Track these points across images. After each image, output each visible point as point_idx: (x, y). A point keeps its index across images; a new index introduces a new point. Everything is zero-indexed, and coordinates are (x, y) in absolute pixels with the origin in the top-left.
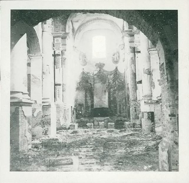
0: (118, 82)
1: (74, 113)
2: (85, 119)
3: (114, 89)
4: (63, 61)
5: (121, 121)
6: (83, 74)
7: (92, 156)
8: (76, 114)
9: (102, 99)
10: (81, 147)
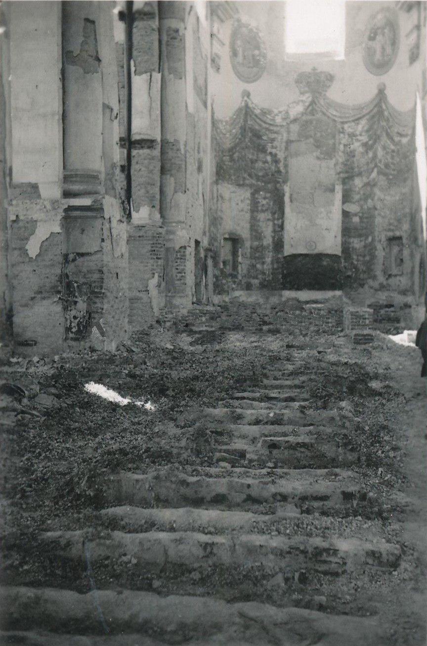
0: (384, 148)
1: (205, 269)
2: (250, 295)
3: (365, 180)
4: (164, 42)
5: (391, 306)
6: (246, 114)
7: (304, 445)
8: (215, 276)
9: (318, 221)
10: (237, 399)
